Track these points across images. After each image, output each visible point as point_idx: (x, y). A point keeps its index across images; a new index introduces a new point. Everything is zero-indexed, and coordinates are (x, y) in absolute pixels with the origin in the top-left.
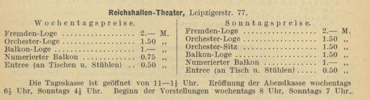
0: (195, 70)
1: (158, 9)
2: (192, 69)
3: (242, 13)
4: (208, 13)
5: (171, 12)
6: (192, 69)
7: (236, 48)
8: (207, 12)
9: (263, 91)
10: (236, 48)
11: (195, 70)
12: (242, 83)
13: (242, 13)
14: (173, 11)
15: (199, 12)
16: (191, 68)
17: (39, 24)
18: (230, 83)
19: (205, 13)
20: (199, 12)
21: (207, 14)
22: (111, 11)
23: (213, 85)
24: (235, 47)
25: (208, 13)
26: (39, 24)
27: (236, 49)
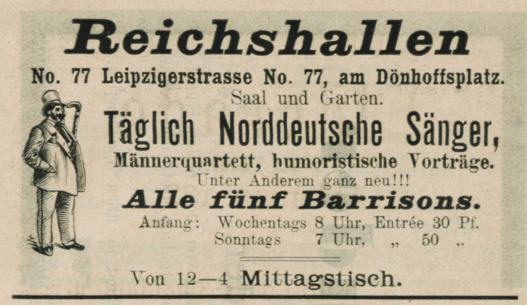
0: (274, 223)
1: (235, 56)
2: (388, 221)
3: (314, 78)
4: (150, 77)
5: (344, 77)
6: (388, 221)
7: (353, 184)
8: (148, 74)
9: (323, 222)
10: (353, 184)
11: (274, 223)
12: (187, 223)
13: (314, 78)
14: (483, 72)
15: (127, 74)
16: (387, 218)
17: (228, 225)
18: (392, 222)
19: (142, 78)
20: (127, 74)
21: (147, 80)
22: (162, 84)
23: (384, 227)
24: (352, 182)
25: (150, 77)
26: (228, 225)
27: (355, 185)
